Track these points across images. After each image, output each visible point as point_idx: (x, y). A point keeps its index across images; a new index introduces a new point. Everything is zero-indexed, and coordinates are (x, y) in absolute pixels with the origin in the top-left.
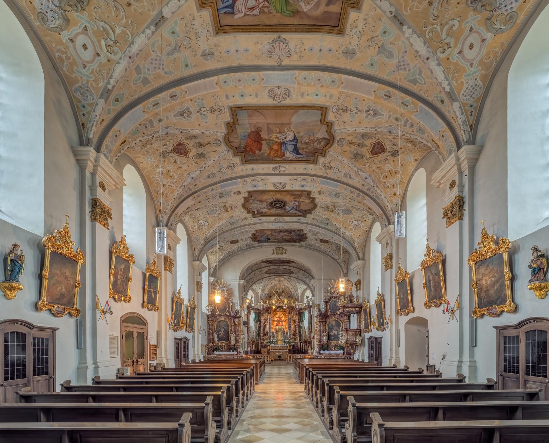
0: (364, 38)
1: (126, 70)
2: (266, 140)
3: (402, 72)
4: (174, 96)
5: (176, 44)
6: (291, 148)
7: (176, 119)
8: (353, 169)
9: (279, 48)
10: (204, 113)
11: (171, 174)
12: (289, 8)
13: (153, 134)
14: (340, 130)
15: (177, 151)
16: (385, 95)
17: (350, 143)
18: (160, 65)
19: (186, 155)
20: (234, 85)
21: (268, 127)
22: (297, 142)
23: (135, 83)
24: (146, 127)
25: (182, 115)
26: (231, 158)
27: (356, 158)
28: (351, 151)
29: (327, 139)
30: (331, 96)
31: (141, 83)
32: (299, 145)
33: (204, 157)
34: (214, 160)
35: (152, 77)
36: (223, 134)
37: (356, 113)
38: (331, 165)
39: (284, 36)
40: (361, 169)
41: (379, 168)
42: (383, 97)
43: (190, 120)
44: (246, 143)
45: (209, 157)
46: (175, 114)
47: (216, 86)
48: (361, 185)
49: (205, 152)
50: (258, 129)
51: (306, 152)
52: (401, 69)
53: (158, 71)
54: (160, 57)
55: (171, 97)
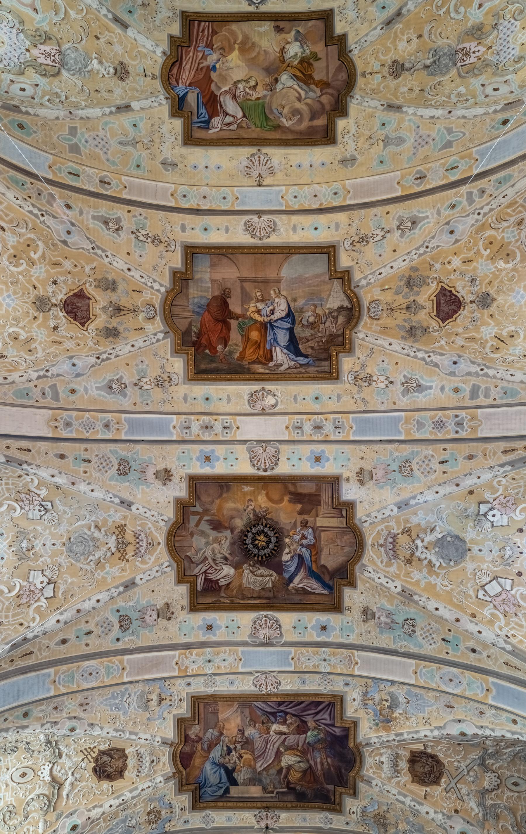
0: (362, 140)
1: (57, 118)
2: (237, 317)
3: (426, 147)
4: (105, 183)
6: (283, 337)
7: (94, 224)
8: (416, 357)
10: (141, 238)
11: (33, 346)
12: (269, 123)
14: (365, 278)
15: (70, 308)
16: (416, 179)
17: (391, 309)
18: (104, 146)
19: (83, 325)
20: (196, 202)
21: (242, 288)
22: (293, 323)
25: (106, 223)
27: (415, 336)
28: (397, 325)
30: (337, 226)
32: (298, 329)
34: (133, 346)
36: (163, 290)
37: (384, 237)
38: (369, 371)
39: (265, 150)
40: (433, 352)
41: (472, 339)
42: (413, 183)
43: (116, 239)
45: (126, 338)
46: (96, 214)
47: (170, 197)
49: (121, 329)
50: (224, 291)
51: (312, 348)
52: (422, 146)
53: (97, 150)
54: (108, 139)
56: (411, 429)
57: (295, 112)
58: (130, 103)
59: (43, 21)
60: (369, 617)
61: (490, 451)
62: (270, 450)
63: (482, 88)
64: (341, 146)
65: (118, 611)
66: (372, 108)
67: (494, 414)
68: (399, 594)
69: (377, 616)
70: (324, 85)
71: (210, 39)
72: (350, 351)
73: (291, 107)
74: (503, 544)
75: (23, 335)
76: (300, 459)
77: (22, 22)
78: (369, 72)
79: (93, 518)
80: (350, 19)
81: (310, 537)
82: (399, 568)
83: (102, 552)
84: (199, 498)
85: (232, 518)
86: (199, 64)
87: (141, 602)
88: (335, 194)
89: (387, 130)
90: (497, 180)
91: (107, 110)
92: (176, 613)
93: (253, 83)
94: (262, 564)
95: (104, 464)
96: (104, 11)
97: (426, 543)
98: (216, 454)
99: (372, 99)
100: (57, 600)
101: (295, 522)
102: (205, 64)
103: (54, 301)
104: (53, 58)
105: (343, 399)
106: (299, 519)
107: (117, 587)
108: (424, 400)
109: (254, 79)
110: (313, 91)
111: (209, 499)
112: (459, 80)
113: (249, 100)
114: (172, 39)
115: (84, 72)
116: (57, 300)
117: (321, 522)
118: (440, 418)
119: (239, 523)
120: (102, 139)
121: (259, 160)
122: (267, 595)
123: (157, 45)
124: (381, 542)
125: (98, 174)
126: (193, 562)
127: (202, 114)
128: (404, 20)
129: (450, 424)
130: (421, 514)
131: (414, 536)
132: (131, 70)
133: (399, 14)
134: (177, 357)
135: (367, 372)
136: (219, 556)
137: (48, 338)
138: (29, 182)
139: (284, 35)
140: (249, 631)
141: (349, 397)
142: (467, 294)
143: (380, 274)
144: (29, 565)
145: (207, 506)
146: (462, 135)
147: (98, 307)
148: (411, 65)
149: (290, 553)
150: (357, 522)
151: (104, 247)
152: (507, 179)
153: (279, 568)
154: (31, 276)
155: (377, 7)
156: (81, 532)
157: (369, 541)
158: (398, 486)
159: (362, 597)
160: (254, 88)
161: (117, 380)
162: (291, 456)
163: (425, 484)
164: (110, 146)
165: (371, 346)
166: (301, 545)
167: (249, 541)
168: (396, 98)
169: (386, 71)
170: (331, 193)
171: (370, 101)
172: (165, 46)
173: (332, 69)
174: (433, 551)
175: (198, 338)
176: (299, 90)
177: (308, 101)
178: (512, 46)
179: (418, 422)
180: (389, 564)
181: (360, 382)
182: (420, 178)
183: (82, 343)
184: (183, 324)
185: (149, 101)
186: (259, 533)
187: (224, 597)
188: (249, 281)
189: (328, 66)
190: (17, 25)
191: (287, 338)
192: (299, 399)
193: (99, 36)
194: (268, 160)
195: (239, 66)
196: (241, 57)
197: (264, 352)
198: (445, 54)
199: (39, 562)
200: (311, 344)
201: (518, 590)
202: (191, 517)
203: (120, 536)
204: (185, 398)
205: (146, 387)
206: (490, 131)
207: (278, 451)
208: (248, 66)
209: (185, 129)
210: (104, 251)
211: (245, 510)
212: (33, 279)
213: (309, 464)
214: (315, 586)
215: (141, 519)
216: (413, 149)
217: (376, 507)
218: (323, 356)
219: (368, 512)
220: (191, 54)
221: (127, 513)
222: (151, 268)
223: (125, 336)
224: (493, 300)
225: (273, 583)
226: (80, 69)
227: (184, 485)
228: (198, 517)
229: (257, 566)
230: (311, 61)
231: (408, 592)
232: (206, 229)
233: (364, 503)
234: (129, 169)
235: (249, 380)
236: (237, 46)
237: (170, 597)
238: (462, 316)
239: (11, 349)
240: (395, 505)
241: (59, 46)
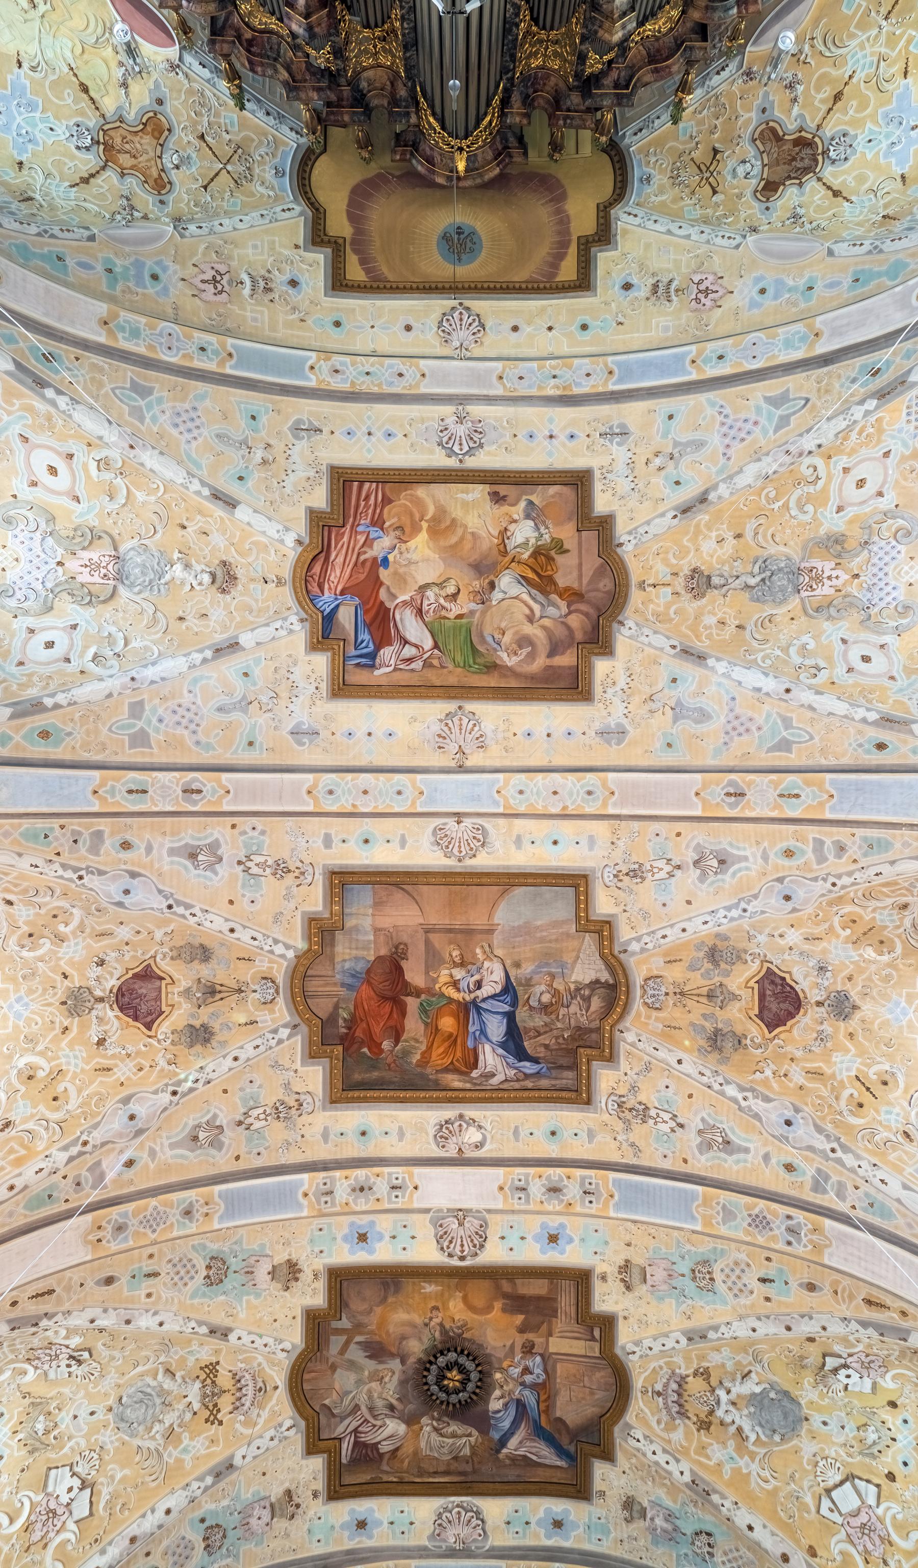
0: (636, 700)
1: (110, 695)
2: (417, 993)
3: (745, 737)
4: (193, 791)
5: (244, 697)
6: (496, 1028)
8: (722, 1093)
12: (478, 660)
13: (83, 873)
14: (638, 939)
16: (728, 794)
17: (682, 994)
18: (191, 721)
21: (428, 942)
22: (514, 1003)
24: (75, 841)
25: (193, 856)
26: (298, 1065)
28: (692, 1024)
29: (606, 985)
30: (592, 840)
32: (521, 1015)
33: (207, 1041)
34: (236, 1059)
35: (161, 738)
36: (291, 954)
37: (671, 875)
38: (642, 1097)
39: (470, 706)
44: (356, 1007)
45: (223, 1044)
46: (176, 845)
47: (306, 797)
48: (782, 1172)
49: (216, 1025)
50: (397, 947)
51: (546, 1047)
52: (740, 735)
53: (179, 731)
55: (185, 791)
56: (712, 1217)
57: (524, 641)
58: (237, 637)
59: (88, 512)
60: (635, 1515)
61: (844, 1290)
62: (472, 1224)
63: (843, 647)
65: (203, 1521)
66: (656, 648)
67: (852, 1238)
68: (687, 1485)
69: (649, 1516)
70: (573, 596)
72: (611, 1058)
73: (516, 633)
74: (864, 1420)
75: (44, 1067)
76: (522, 1238)
77: (52, 519)
78: (651, 581)
79: (162, 1359)
81: (537, 1371)
82: (688, 1435)
83: (177, 1414)
84: (347, 1305)
85: (403, 1338)
87: (243, 1497)
88: (589, 793)
90: (865, 839)
91: (197, 657)
92: (303, 1506)
93: (451, 590)
94: (453, 1416)
95: (182, 1273)
96: (196, 486)
97: (733, 1396)
98: (378, 1228)
99: (655, 632)
100: (95, 1521)
101: (512, 1346)
102: (370, 554)
103: (98, 993)
104: (103, 571)
105: (599, 1138)
106: (520, 1340)
107: (201, 1479)
108: (735, 1168)
109: (453, 582)
110: (554, 605)
111: (363, 1307)
112: (803, 618)
113: (445, 618)
114: (314, 516)
116: (104, 990)
117: (557, 1345)
118: (761, 1212)
119: (416, 1348)
122: (461, 1469)
124: (659, 1387)
126: (333, 1415)
128: (712, 509)
129: (779, 1227)
130: (726, 1351)
131: (714, 1382)
132: (239, 572)
133: (703, 499)
134: (313, 1064)
135: (639, 1099)
136: (379, 1403)
137: (87, 1063)
138: (56, 826)
139: (506, 508)
140: (429, 1529)
141: (609, 1139)
142: (811, 989)
143: (664, 937)
144: (48, 1460)
145: (360, 1318)
147: (176, 990)
148: (723, 582)
149: (502, 1397)
150: (618, 1351)
151: (188, 901)
153: (483, 1423)
154: (59, 959)
155: (666, 478)
156: (140, 1384)
157: (638, 1382)
158: (690, 1302)
159: (623, 1480)
160: (454, 597)
161: (208, 1123)
162: (507, 1232)
163: (734, 1309)
164: (202, 718)
165: (647, 1058)
166: (523, 1384)
167: (431, 1379)
168: (697, 637)
169: (679, 584)
170: (582, 792)
172: (301, 528)
173: (588, 572)
174: (745, 1412)
175: (349, 1028)
176: (531, 603)
177: (546, 622)
178: (893, 583)
179: (724, 1207)
180: (670, 1427)
181: (627, 1114)
182: (736, 795)
183: (146, 1064)
184: (323, 1007)
185: (271, 629)
186: (449, 1367)
187: (387, 1473)
188: (440, 931)
190: (43, 525)
191: (503, 1029)
192: (522, 1134)
195: (428, 560)
197: (463, 1052)
198: (780, 570)
199: (66, 1450)
200: (545, 1039)
201: (888, 1508)
202: (333, 1338)
203: (209, 1381)
204: (325, 1135)
205: (257, 1125)
207: (484, 1225)
208: (444, 560)
210: (188, 906)
211: (426, 1325)
212: (62, 963)
213: (538, 1246)
214: (545, 1454)
215: (245, 1352)
217: (652, 1331)
218: (564, 1061)
219: (637, 1338)
220: (345, 539)
221: (222, 1345)
222: (271, 920)
223: (222, 1039)
224: (855, 1007)
225: (472, 1447)
226: (151, 581)
227: (321, 1285)
228: (345, 1338)
229: (446, 1419)
230: (553, 553)
231: (702, 1486)
232: (366, 841)
233: (631, 1320)
234: (235, 752)
235: (438, 1100)
236: (425, 525)
237: (293, 1480)
238: (802, 1025)
239: (21, 1102)
240: (684, 1333)
241: (116, 549)
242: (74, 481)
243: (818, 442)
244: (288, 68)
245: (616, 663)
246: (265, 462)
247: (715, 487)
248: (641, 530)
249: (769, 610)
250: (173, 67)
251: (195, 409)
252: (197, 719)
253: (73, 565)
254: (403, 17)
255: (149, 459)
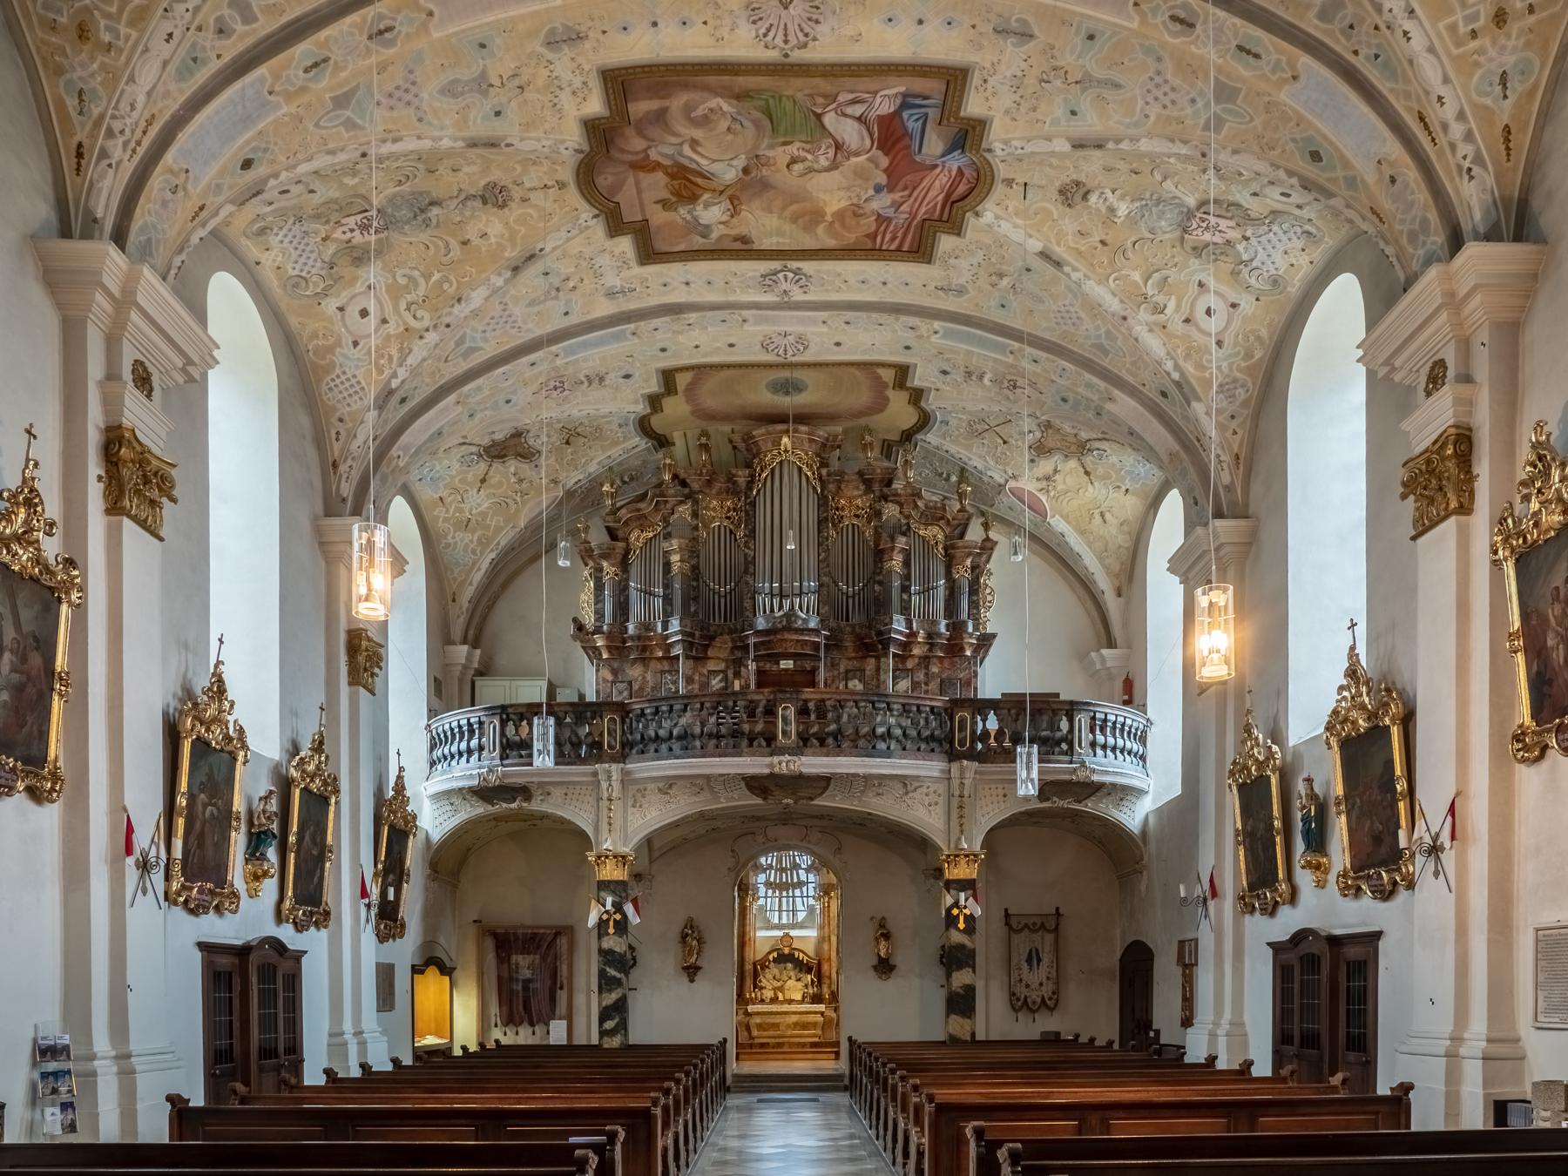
1: (1235, 152)
4: (1182, 21)
9: (786, 29)
12: (762, 103)
16: (389, 29)
18: (1157, 86)
23: (1248, 119)
24: (1351, 27)
31: (1238, 102)
52: (398, 88)
55: (1192, 26)
57: (705, 121)
64: (587, 68)
71: (882, 228)
77: (1235, 274)
80: (607, 256)
86: (910, 196)
89: (488, 106)
90: (205, 62)
91: (1125, 146)
93: (797, 167)
102: (897, 196)
104: (1204, 225)
110: (666, 156)
115: (1151, 199)
120: (1156, 99)
121: (786, 35)
123: (989, 226)
125: (1192, 43)
127: (917, 120)
132: (1055, 195)
138: (1361, 57)
139: (733, 232)
146: (321, 123)
152: (184, 74)
155: (558, 274)
160: (794, 161)
169: (517, 193)
171: (539, 148)
176: (695, 157)
177: (674, 140)
182: (381, 33)
185: (1028, 149)
189: (639, 192)
190: (1245, 271)
193: (1099, 245)
194: (765, 35)
196: (821, 204)
198: (407, 222)
206: (267, 143)
209: (961, 97)
216: (418, 80)
220: (923, 210)
230: (674, 199)
242: (1195, 299)
243: (424, 341)
244: (916, 506)
245: (576, 113)
246: (1001, 276)
247: (507, 282)
248: (574, 232)
249: (406, 188)
250: (1014, 477)
251: (1057, 324)
252: (1150, 86)
253: (1233, 235)
254: (827, 539)
255: (1113, 304)
